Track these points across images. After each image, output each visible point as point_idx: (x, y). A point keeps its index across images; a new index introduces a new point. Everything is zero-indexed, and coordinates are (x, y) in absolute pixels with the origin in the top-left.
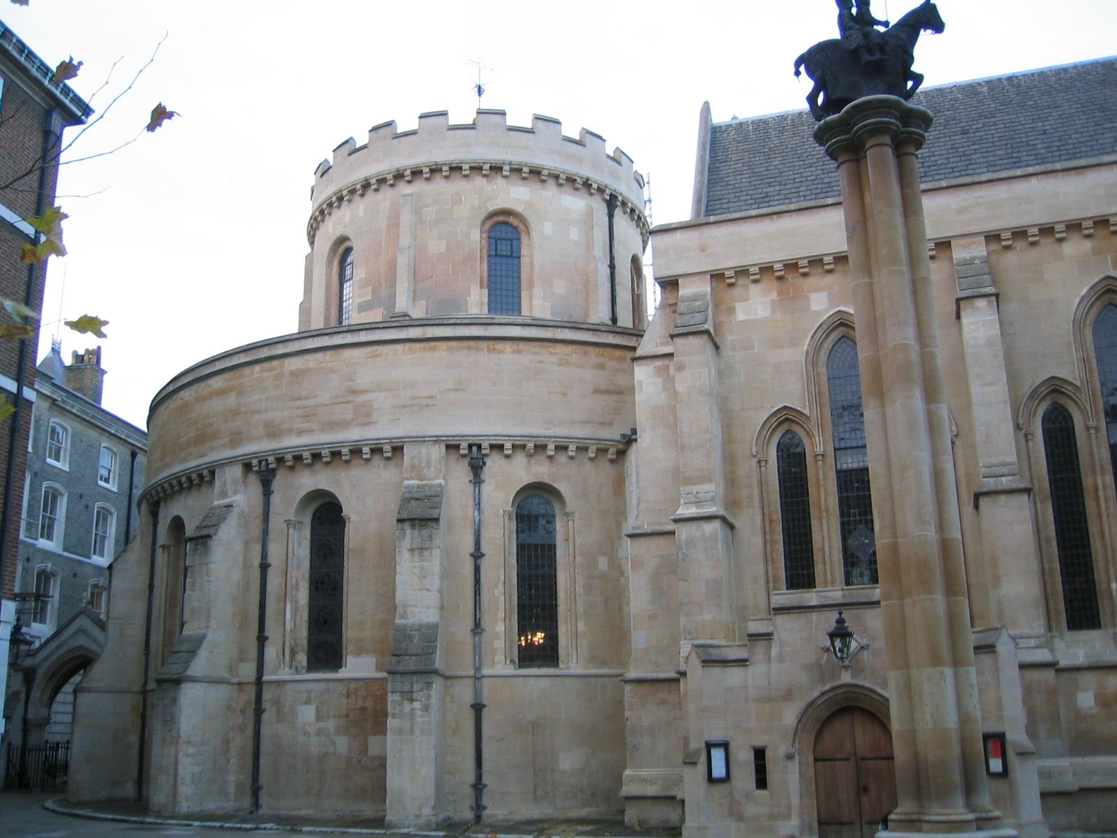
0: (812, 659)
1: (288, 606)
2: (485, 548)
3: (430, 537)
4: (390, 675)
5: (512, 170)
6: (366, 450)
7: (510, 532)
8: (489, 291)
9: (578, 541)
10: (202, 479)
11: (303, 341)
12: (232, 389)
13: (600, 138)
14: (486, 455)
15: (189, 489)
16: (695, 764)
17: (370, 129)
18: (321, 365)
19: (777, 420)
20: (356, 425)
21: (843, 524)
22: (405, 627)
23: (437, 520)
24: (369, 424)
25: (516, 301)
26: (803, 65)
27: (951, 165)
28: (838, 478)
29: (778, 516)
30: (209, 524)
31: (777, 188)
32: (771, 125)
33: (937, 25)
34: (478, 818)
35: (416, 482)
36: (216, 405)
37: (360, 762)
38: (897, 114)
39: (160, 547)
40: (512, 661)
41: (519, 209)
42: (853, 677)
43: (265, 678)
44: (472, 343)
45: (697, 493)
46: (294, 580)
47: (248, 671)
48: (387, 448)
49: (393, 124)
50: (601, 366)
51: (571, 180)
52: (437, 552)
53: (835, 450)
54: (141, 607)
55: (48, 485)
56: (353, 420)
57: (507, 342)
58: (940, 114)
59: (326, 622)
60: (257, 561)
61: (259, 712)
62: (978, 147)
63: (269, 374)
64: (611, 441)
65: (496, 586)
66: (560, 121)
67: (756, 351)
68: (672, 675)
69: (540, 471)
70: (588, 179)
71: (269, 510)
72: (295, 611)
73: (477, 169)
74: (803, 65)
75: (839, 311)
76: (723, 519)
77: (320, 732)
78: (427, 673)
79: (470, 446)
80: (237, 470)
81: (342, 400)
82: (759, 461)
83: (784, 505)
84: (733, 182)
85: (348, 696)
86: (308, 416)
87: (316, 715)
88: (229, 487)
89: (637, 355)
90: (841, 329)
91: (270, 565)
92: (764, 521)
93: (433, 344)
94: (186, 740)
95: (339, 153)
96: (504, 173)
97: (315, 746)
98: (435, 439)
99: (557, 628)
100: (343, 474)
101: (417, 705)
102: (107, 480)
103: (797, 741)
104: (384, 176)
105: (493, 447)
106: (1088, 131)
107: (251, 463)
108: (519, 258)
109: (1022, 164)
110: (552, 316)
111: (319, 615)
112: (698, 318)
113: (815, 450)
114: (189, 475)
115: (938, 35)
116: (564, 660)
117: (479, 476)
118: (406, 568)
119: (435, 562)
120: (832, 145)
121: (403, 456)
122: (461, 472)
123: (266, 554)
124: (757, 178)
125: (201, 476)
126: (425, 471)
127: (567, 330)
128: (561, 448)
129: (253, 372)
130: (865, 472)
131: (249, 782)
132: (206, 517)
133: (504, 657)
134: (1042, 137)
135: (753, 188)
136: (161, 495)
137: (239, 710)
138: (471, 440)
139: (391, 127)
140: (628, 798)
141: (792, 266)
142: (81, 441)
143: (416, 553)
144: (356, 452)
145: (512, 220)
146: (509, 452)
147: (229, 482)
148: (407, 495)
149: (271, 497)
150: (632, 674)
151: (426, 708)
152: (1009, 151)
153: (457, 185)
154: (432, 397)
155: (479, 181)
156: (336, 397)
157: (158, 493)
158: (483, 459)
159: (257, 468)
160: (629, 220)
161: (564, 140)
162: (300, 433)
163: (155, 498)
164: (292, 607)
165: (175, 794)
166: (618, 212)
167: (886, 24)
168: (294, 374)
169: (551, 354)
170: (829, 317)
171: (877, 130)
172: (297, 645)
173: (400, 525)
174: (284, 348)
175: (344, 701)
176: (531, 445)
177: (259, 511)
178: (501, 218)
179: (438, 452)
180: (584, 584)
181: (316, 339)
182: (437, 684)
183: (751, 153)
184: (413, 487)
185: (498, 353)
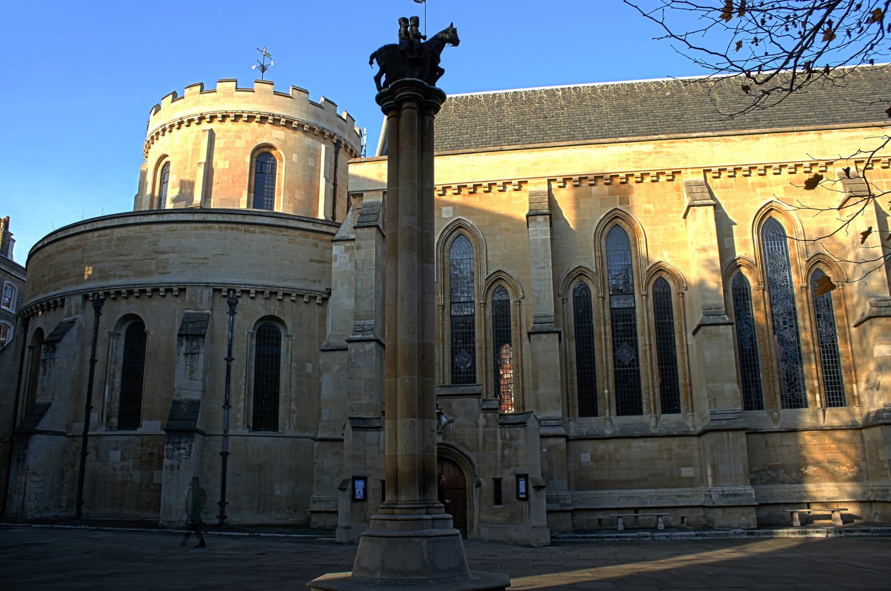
1: (107, 387)
2: (234, 355)
7: (252, 345)
10: (54, 304)
13: (333, 104)
14: (239, 297)
16: (344, 490)
18: (137, 234)
20: (157, 274)
21: (452, 349)
23: (203, 336)
24: (165, 273)
26: (375, 59)
33: (455, 42)
37: (148, 487)
38: (422, 91)
40: (248, 427)
43: (89, 433)
45: (363, 325)
47: (79, 427)
52: (202, 356)
53: (451, 303)
54: (14, 386)
57: (257, 226)
60: (88, 359)
61: (84, 454)
62: (551, 126)
63: (104, 238)
65: (240, 379)
69: (273, 308)
70: (323, 128)
72: (112, 390)
74: (375, 59)
75: (459, 219)
76: (378, 342)
77: (122, 469)
78: (190, 433)
79: (229, 290)
80: (79, 299)
85: (142, 445)
88: (73, 310)
89: (335, 239)
91: (97, 361)
94: (33, 471)
102: (8, 305)
104: (192, 118)
105: (243, 291)
106: (615, 123)
107: (88, 295)
109: (575, 138)
110: (294, 212)
112: (373, 218)
117: (233, 309)
118: (181, 365)
120: (387, 105)
122: (223, 306)
125: (56, 302)
134: (588, 124)
138: (230, 286)
140: (313, 512)
143: (189, 356)
144: (156, 290)
146: (253, 295)
149: (100, 317)
150: (320, 435)
152: (569, 130)
154: (206, 258)
156: (146, 255)
159: (92, 298)
160: (349, 156)
162: (121, 277)
163: (26, 316)
164: (109, 387)
166: (342, 150)
167: (425, 38)
168: (119, 239)
169: (284, 235)
176: (267, 292)
179: (207, 293)
182: (198, 438)
185: (251, 233)
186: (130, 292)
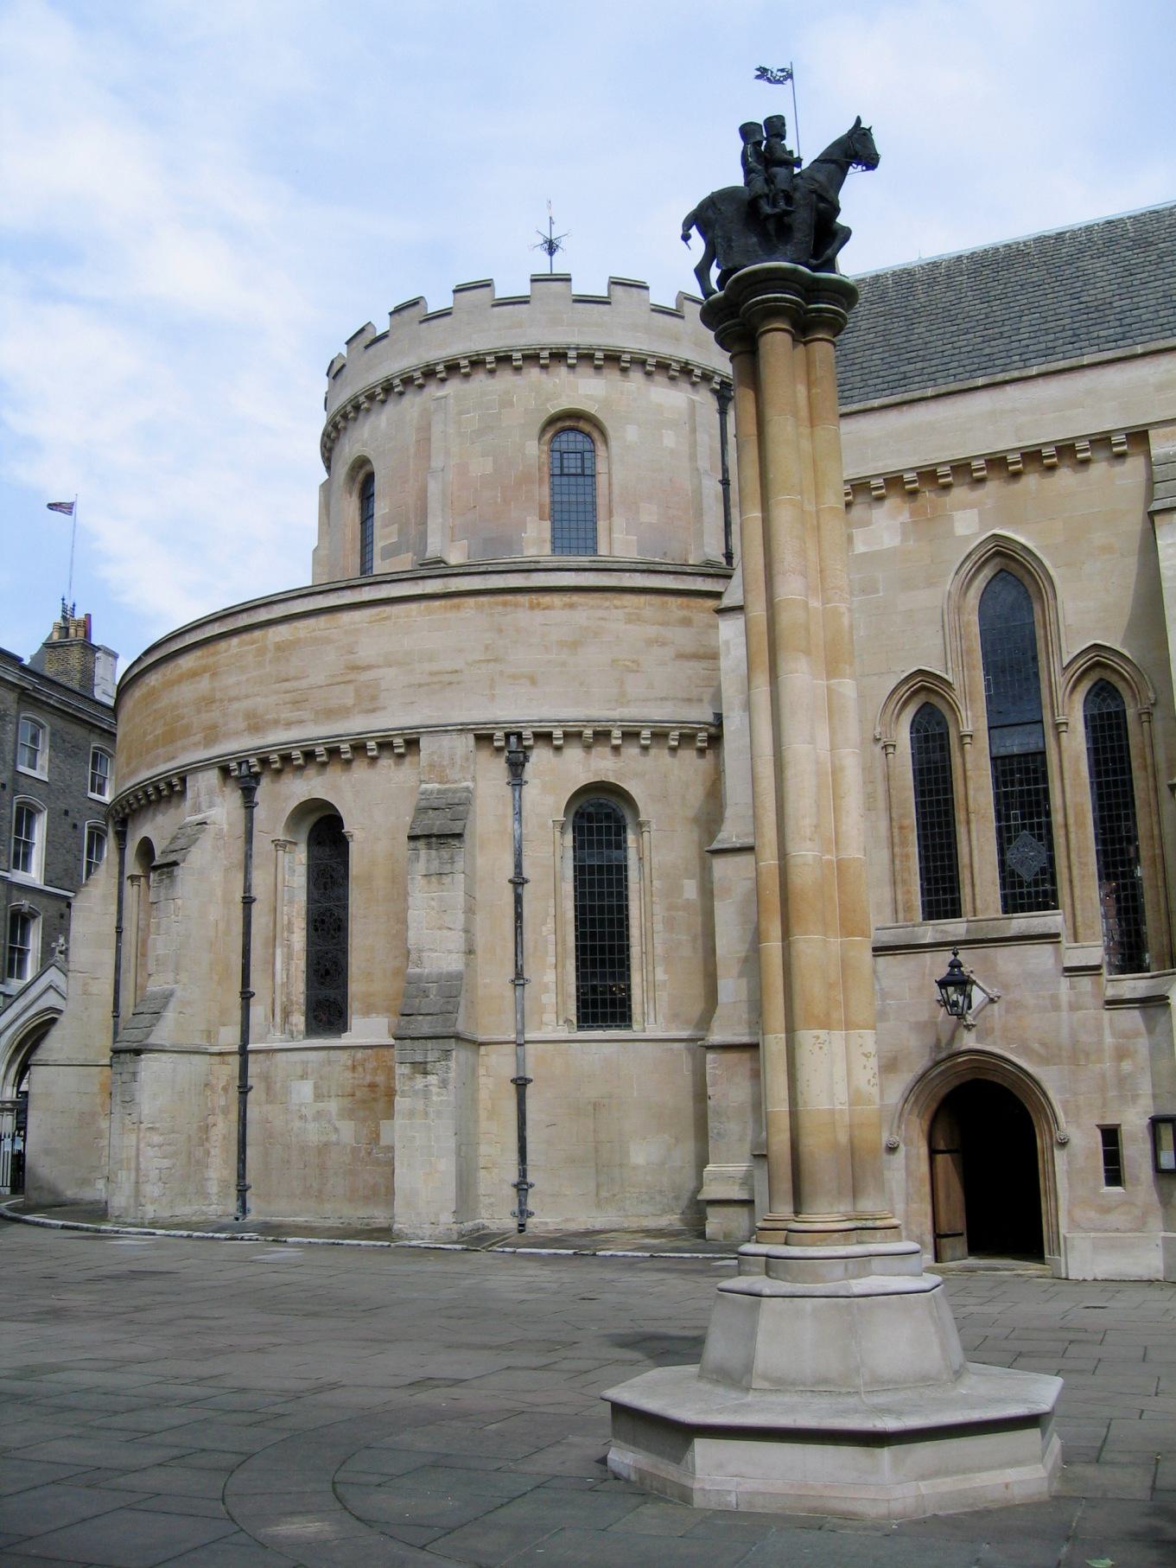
0: (924, 1016)
1: (279, 952)
3: (452, 858)
4: (398, 1041)
5: (580, 357)
6: (371, 744)
8: (553, 523)
9: (655, 861)
11: (290, 604)
12: (205, 669)
15: (169, 798)
17: (392, 309)
19: (910, 688)
20: (359, 713)
21: (999, 830)
22: (419, 978)
24: (374, 711)
25: (590, 535)
26: (694, 228)
27: (1161, 321)
28: (994, 766)
29: (911, 820)
30: (177, 849)
31: (919, 365)
32: (917, 276)
34: (522, 1228)
35: (437, 786)
36: (187, 692)
39: (128, 878)
41: (591, 408)
42: (979, 1039)
43: (251, 1046)
44: (509, 598)
46: (286, 918)
47: (229, 1038)
48: (398, 741)
49: (422, 303)
50: (686, 622)
51: (663, 366)
55: (21, 800)
56: (354, 705)
58: (1152, 248)
59: (327, 972)
60: (239, 894)
61: (244, 1090)
64: (699, 723)
65: (544, 923)
66: (648, 284)
67: (881, 594)
68: (522, 1042)
69: (600, 766)
70: (687, 363)
71: (252, 828)
72: (289, 957)
73: (532, 358)
74: (694, 228)
75: (994, 535)
77: (319, 1115)
79: (507, 736)
80: (213, 776)
81: (339, 679)
82: (885, 747)
83: (920, 806)
84: (860, 360)
86: (297, 702)
87: (315, 1094)
88: (204, 799)
90: (997, 560)
92: (891, 827)
93: (456, 601)
95: (354, 345)
96: (570, 361)
97: (313, 1133)
98: (460, 727)
99: (629, 976)
100: (343, 778)
101: (432, 1079)
103: (903, 1127)
108: (593, 476)
111: (319, 963)
113: (961, 729)
114: (157, 784)
115: (870, 172)
116: (639, 1019)
119: (456, 892)
121: (420, 751)
122: (497, 768)
123: (250, 886)
124: (893, 353)
126: (448, 771)
127: (638, 574)
128: (631, 735)
129: (229, 646)
130: (1039, 757)
131: (234, 1179)
132: (174, 839)
133: (555, 1016)
135: (886, 366)
136: (127, 811)
137: (220, 1087)
139: (417, 307)
141: (929, 475)
142: (64, 741)
144: (359, 748)
145: (582, 425)
147: (203, 792)
148: (423, 804)
151: (444, 1084)
153: (505, 380)
155: (534, 373)
157: (124, 809)
158: (524, 753)
161: (653, 310)
162: (289, 724)
164: (282, 952)
165: (137, 1193)
168: (279, 647)
170: (987, 539)
171: (773, 311)
172: (292, 1004)
173: (411, 843)
174: (267, 613)
175: (348, 1074)
176: (588, 732)
177: (240, 829)
178: (568, 423)
180: (664, 917)
181: (306, 600)
183: (887, 317)
184: (432, 793)
185: (544, 609)
186: (309, 756)
